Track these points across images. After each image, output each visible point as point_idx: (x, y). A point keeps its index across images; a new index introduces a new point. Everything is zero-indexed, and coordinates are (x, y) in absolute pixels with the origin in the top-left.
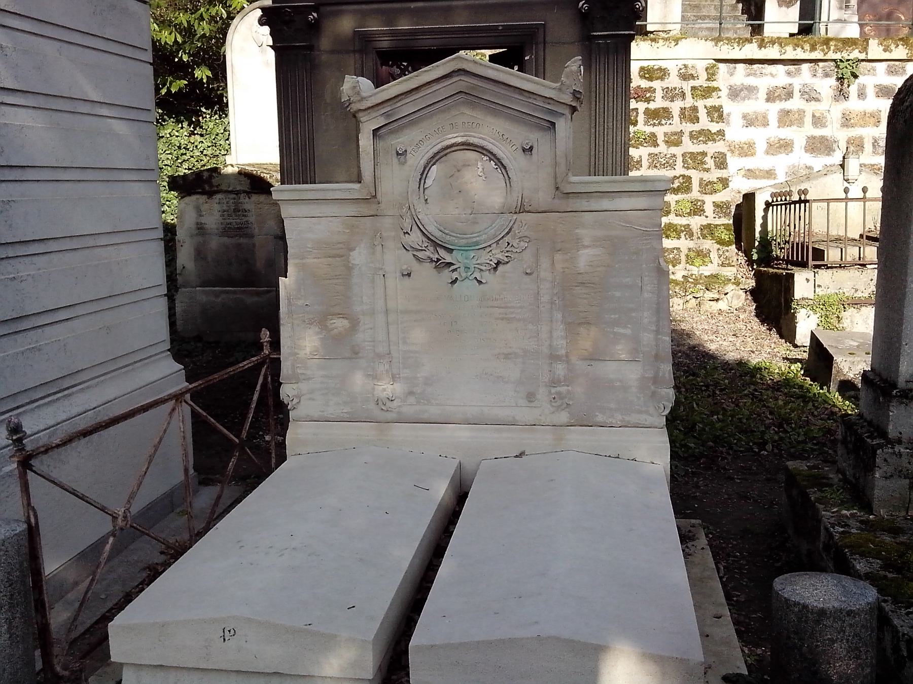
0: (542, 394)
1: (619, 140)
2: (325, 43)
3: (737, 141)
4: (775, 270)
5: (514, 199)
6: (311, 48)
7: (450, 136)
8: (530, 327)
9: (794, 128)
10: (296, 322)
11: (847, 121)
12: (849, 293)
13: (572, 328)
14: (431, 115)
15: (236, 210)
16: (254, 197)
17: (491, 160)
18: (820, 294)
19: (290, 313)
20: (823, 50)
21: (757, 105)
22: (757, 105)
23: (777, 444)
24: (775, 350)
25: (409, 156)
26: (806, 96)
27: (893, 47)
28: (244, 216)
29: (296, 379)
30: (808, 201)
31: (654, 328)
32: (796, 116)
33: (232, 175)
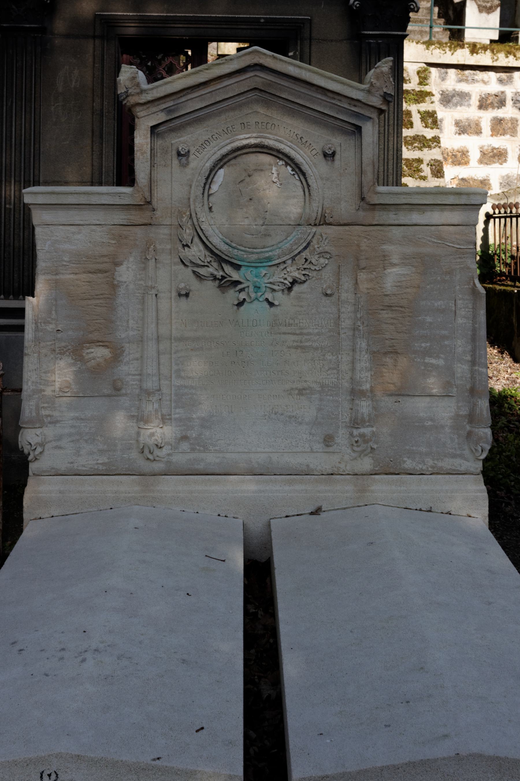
0: (342, 437)
1: (391, 146)
2: (60, 25)
3: (450, 148)
4: (502, 288)
5: (315, 209)
7: (242, 136)
8: (329, 357)
9: (508, 137)
10: (44, 351)
13: (377, 356)
14: (219, 113)
19: (37, 340)
21: (470, 112)
22: (470, 112)
24: (514, 375)
25: (192, 157)
29: (39, 422)
31: (469, 358)
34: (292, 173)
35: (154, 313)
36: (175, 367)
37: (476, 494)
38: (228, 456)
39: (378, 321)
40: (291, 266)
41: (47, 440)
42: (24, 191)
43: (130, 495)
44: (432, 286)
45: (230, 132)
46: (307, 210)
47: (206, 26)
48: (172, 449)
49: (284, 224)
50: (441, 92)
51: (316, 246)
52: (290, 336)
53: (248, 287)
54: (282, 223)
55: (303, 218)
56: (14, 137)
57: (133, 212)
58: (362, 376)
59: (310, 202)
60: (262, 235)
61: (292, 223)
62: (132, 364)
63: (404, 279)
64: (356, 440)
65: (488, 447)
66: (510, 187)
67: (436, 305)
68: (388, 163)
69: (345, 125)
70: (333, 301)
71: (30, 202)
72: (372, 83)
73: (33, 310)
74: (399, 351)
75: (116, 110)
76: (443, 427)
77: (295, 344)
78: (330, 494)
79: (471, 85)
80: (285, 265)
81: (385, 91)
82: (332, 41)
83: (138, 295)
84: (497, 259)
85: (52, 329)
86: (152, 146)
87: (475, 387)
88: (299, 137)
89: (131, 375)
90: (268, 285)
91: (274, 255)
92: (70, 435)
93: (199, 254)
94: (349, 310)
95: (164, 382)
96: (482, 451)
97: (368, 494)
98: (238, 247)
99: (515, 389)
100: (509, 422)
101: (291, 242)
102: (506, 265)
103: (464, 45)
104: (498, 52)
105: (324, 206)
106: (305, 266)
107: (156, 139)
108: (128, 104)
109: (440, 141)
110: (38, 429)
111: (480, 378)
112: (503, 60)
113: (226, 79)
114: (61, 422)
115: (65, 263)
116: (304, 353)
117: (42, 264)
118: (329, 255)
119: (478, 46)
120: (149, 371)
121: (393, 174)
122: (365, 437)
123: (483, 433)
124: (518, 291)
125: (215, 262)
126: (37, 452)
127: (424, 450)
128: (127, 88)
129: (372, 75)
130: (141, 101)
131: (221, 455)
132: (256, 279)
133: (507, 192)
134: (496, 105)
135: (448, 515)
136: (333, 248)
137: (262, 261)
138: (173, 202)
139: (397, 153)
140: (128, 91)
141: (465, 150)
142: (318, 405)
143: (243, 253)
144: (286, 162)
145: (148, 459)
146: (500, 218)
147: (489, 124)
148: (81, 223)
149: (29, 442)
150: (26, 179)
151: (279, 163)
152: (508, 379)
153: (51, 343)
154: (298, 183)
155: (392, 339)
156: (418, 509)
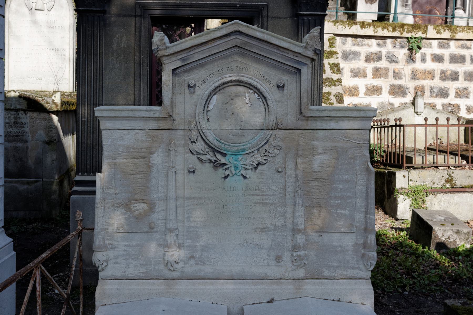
0: (287, 257)
1: (316, 82)
2: (114, 9)
5: (272, 120)
6: (104, 12)
7: (227, 75)
8: (279, 209)
11: (414, 76)
12: (429, 185)
13: (308, 208)
14: (214, 61)
15: (16, 123)
16: (30, 114)
17: (255, 92)
18: (412, 185)
19: (103, 199)
20: (400, 31)
21: (360, 64)
22: (360, 64)
23: (412, 286)
24: (385, 222)
25: (197, 88)
26: (389, 60)
27: (442, 31)
28: (20, 127)
29: (105, 248)
30: (402, 126)
31: (364, 210)
32: (384, 72)
33: (14, 98)
34: (258, 98)
35: (174, 183)
36: (186, 215)
38: (218, 268)
46: (267, 121)
47: (203, 9)
52: (256, 196)
57: (161, 122)
63: (325, 162)
67: (344, 178)
71: (99, 116)
73: (101, 181)
74: (322, 206)
76: (347, 251)
77: (259, 201)
80: (253, 154)
82: (280, 18)
87: (367, 228)
88: (262, 76)
90: (243, 166)
92: (123, 255)
93: (201, 147)
95: (180, 224)
100: (383, 249)
102: (381, 156)
103: (357, 23)
104: (378, 27)
106: (265, 154)
112: (381, 32)
117: (106, 153)
120: (171, 218)
126: (103, 266)
130: (166, 54)
131: (214, 267)
143: (228, 146)
144: (254, 91)
145: (170, 270)
146: (377, 128)
148: (130, 128)
150: (94, 103)
152: (381, 224)
154: (262, 104)
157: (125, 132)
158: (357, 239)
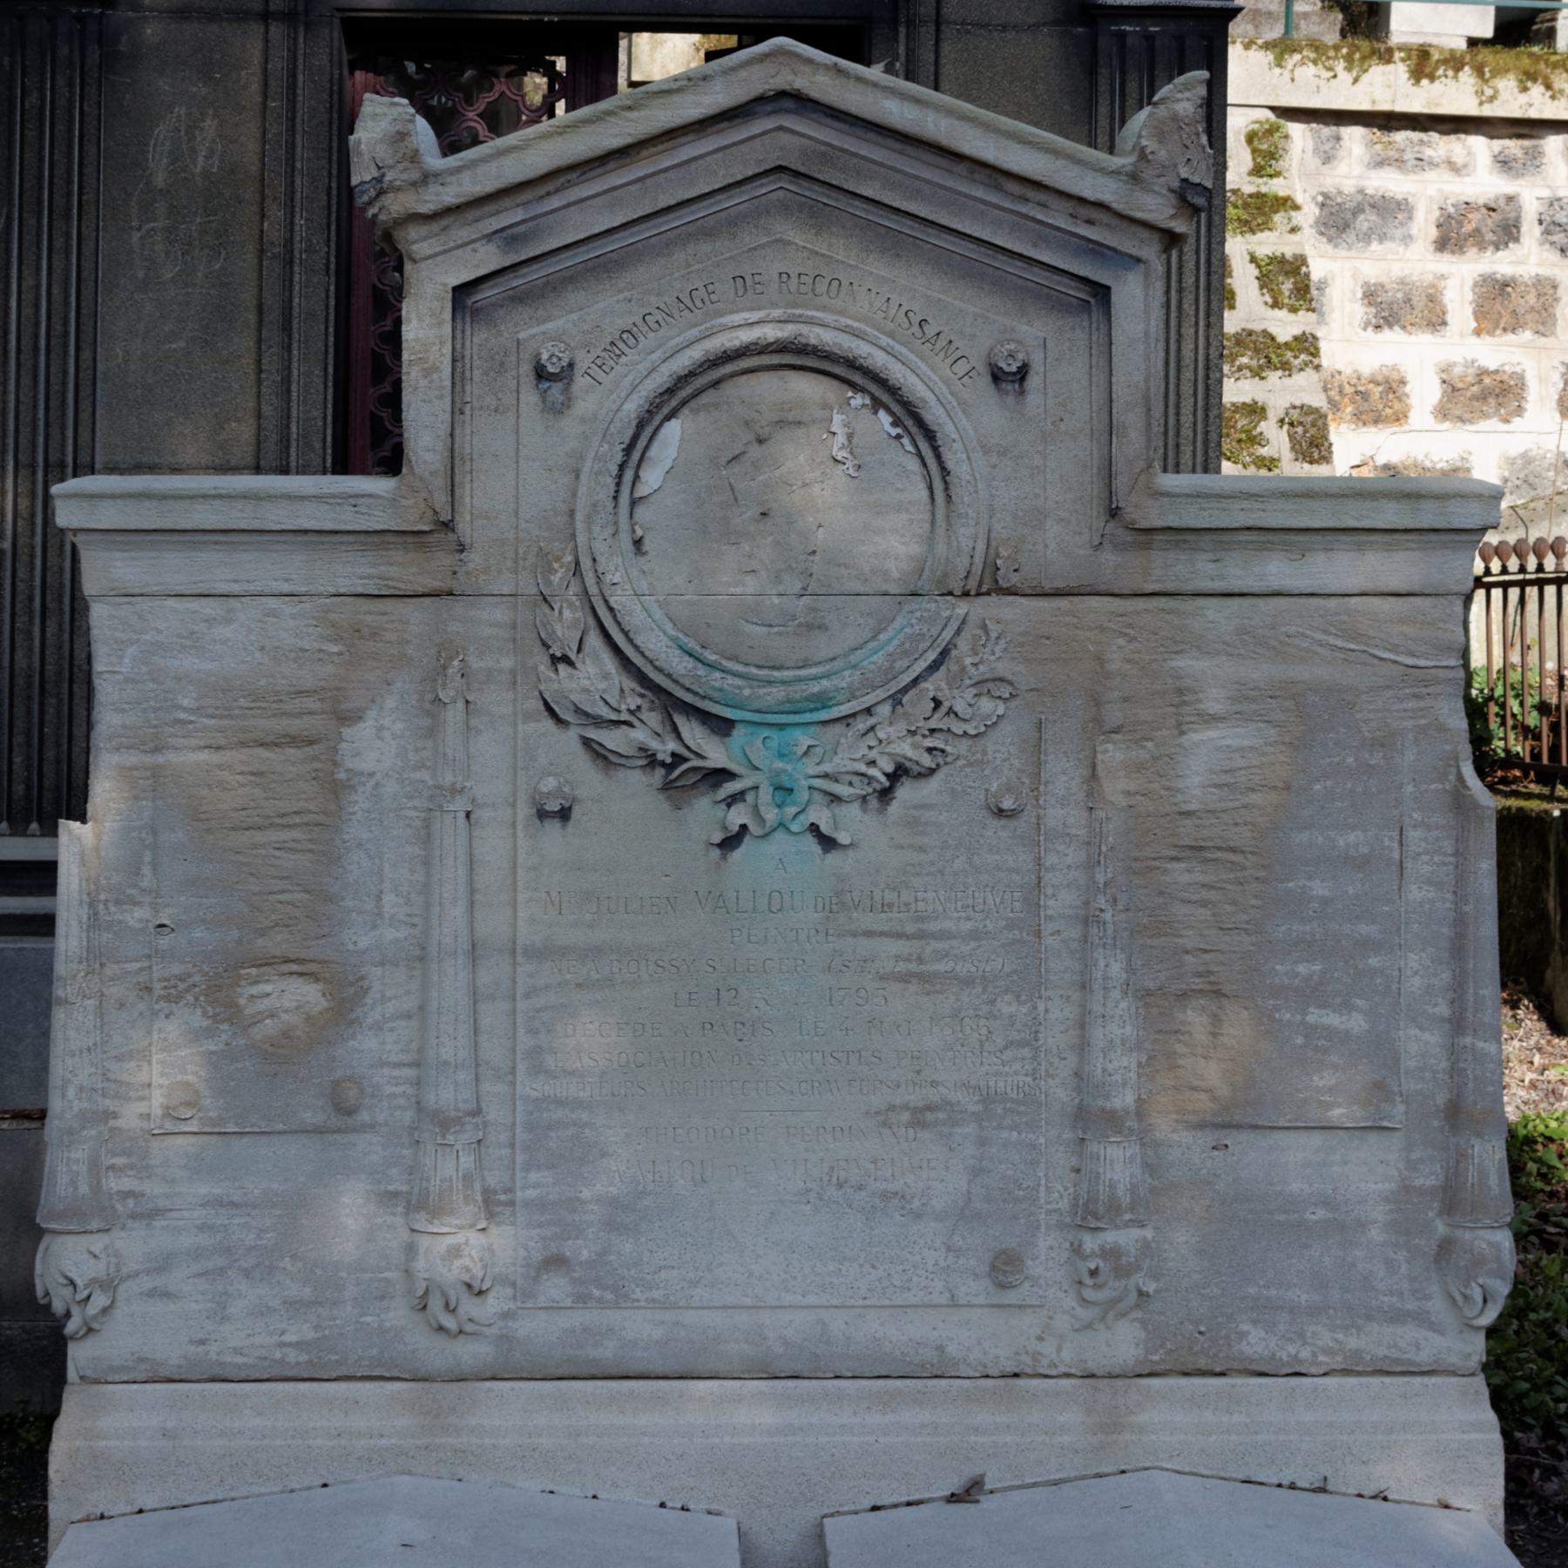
0: (1047, 1257)
3: (1348, 371)
5: (964, 545)
7: (738, 318)
8: (1007, 1007)
9: (1527, 335)
13: (1159, 1004)
17: (877, 404)
19: (95, 957)
21: (1410, 259)
22: (1410, 259)
24: (1552, 1074)
25: (581, 382)
29: (100, 1214)
31: (1443, 1009)
32: (1532, 299)
34: (894, 431)
35: (462, 871)
36: (525, 1041)
37: (1465, 1437)
38: (690, 1317)
39: (1161, 893)
40: (891, 724)
41: (124, 1271)
42: (55, 489)
43: (383, 1442)
44: (1329, 783)
45: (699, 304)
46: (941, 549)
48: (514, 1298)
49: (868, 590)
50: (1320, 199)
51: (968, 661)
52: (886, 940)
53: (757, 788)
54: (861, 589)
55: (927, 572)
56: (13, 328)
57: (397, 556)
58: (1110, 1067)
59: (949, 523)
60: (800, 625)
61: (893, 589)
62: (391, 1030)
64: (1093, 1267)
65: (1503, 1289)
66: (1533, 493)
67: (1342, 843)
68: (1178, 406)
69: (1059, 283)
70: (1019, 832)
72: (1143, 149)
73: (83, 863)
74: (1226, 989)
75: (333, 246)
76: (1362, 1225)
77: (902, 967)
78: (1009, 1439)
79: (1412, 177)
80: (871, 721)
81: (1184, 176)
82: (1004, 28)
83: (413, 814)
84: (1497, 715)
85: (141, 920)
86: (458, 347)
87: (1464, 1105)
88: (916, 320)
89: (388, 1064)
90: (818, 783)
91: (838, 690)
93: (602, 686)
94: (1069, 860)
96: (1485, 1301)
97: (1128, 1437)
98: (724, 662)
99: (1556, 1115)
100: (1543, 1217)
101: (890, 649)
102: (1526, 732)
103: (1390, 51)
104: (1496, 73)
105: (993, 535)
106: (933, 724)
107: (468, 327)
108: (382, 217)
109: (1317, 349)
110: (96, 1236)
111: (1478, 1072)
112: (1511, 100)
113: (690, 138)
114: (169, 1215)
115: (183, 716)
116: (928, 994)
117: (109, 718)
118: (1010, 689)
119: (1436, 56)
120: (447, 1053)
121: (1194, 442)
122: (1119, 1257)
123: (1489, 1243)
124: (1562, 811)
125: (651, 709)
126: (93, 1309)
127: (1304, 1297)
128: (379, 168)
129: (1145, 125)
130: (424, 209)
131: (669, 1316)
132: (779, 765)
133: (1525, 506)
134: (1490, 236)
135: (1379, 1503)
136: (1021, 668)
137: (798, 706)
138: (523, 525)
139: (1207, 377)
140: (383, 175)
141: (1395, 376)
142: (973, 1157)
143: (738, 682)
144: (874, 398)
145: (441, 1328)
146: (1505, 586)
147: (1470, 296)
148: (235, 588)
149: (67, 1278)
150: (52, 459)
151: (852, 402)
152: (1533, 1085)
153: (138, 965)
154: (913, 464)
155: (1205, 951)
156: (1285, 1482)
157: (208, 607)
158: (1412, 1166)
